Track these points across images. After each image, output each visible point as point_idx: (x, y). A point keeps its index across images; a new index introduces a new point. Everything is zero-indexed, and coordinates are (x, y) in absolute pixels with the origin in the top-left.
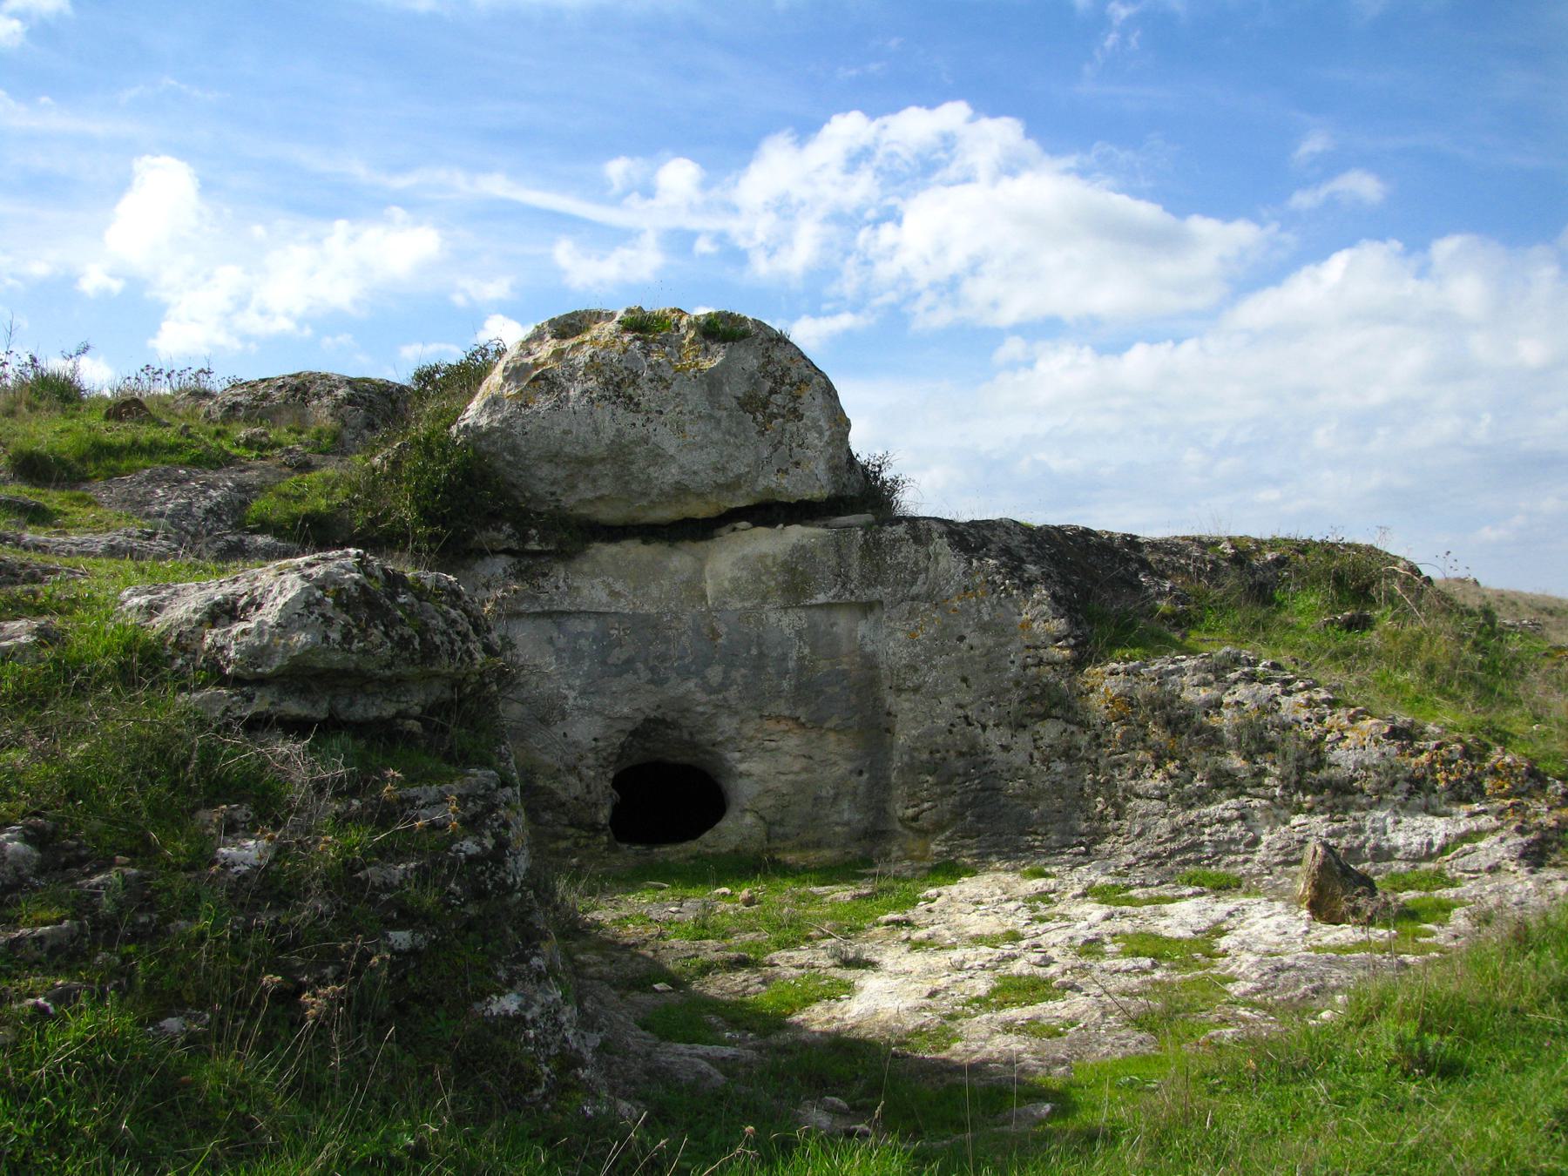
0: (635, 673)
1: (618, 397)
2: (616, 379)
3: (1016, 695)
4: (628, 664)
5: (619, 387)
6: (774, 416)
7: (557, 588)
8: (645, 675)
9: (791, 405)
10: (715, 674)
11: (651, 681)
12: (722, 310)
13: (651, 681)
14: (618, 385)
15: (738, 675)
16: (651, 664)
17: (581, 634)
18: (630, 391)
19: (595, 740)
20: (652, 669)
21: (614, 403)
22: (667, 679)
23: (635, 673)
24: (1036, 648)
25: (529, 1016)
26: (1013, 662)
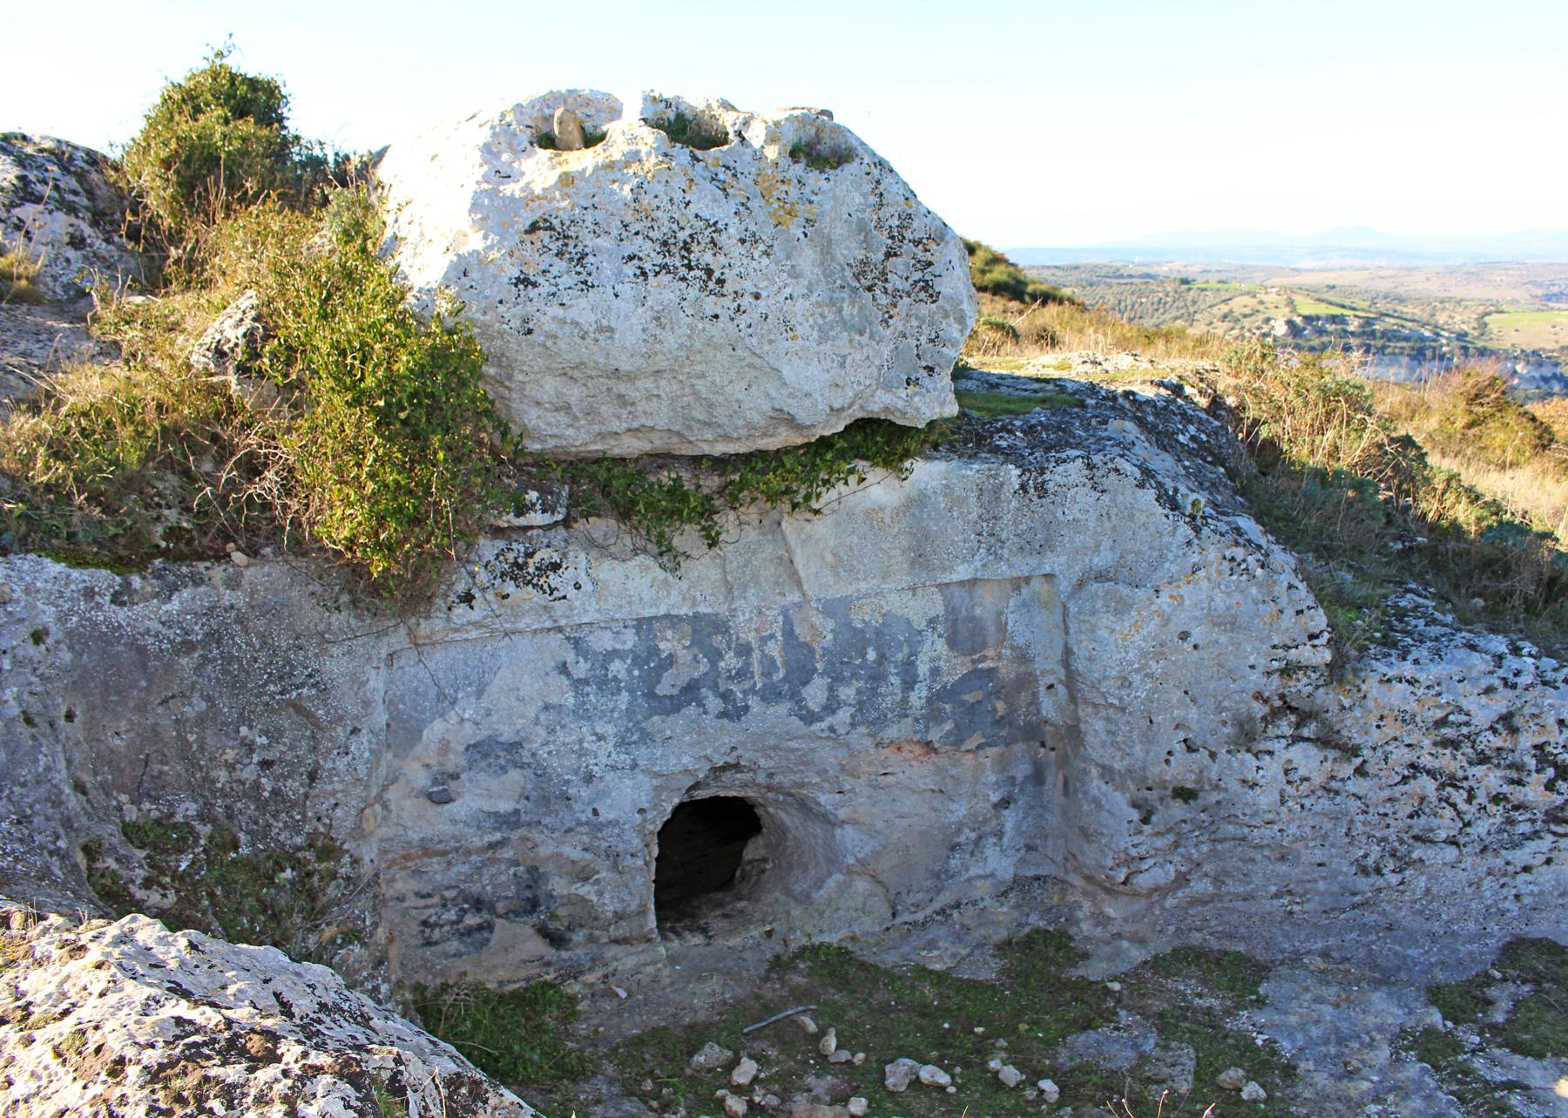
0: (700, 704)
1: (690, 268)
2: (682, 235)
3: (237, 144)
4: (691, 691)
5: (689, 251)
6: (896, 294)
7: (578, 587)
8: (714, 703)
9: (918, 276)
10: (815, 693)
11: (723, 714)
12: (617, 95)
13: (723, 714)
14: (686, 247)
15: (847, 692)
16: (722, 689)
17: (613, 654)
18: (708, 258)
19: (641, 811)
20: (726, 696)
21: (683, 279)
22: (747, 708)
23: (700, 704)
24: (1287, 648)
25: (451, 982)
26: (1252, 667)
